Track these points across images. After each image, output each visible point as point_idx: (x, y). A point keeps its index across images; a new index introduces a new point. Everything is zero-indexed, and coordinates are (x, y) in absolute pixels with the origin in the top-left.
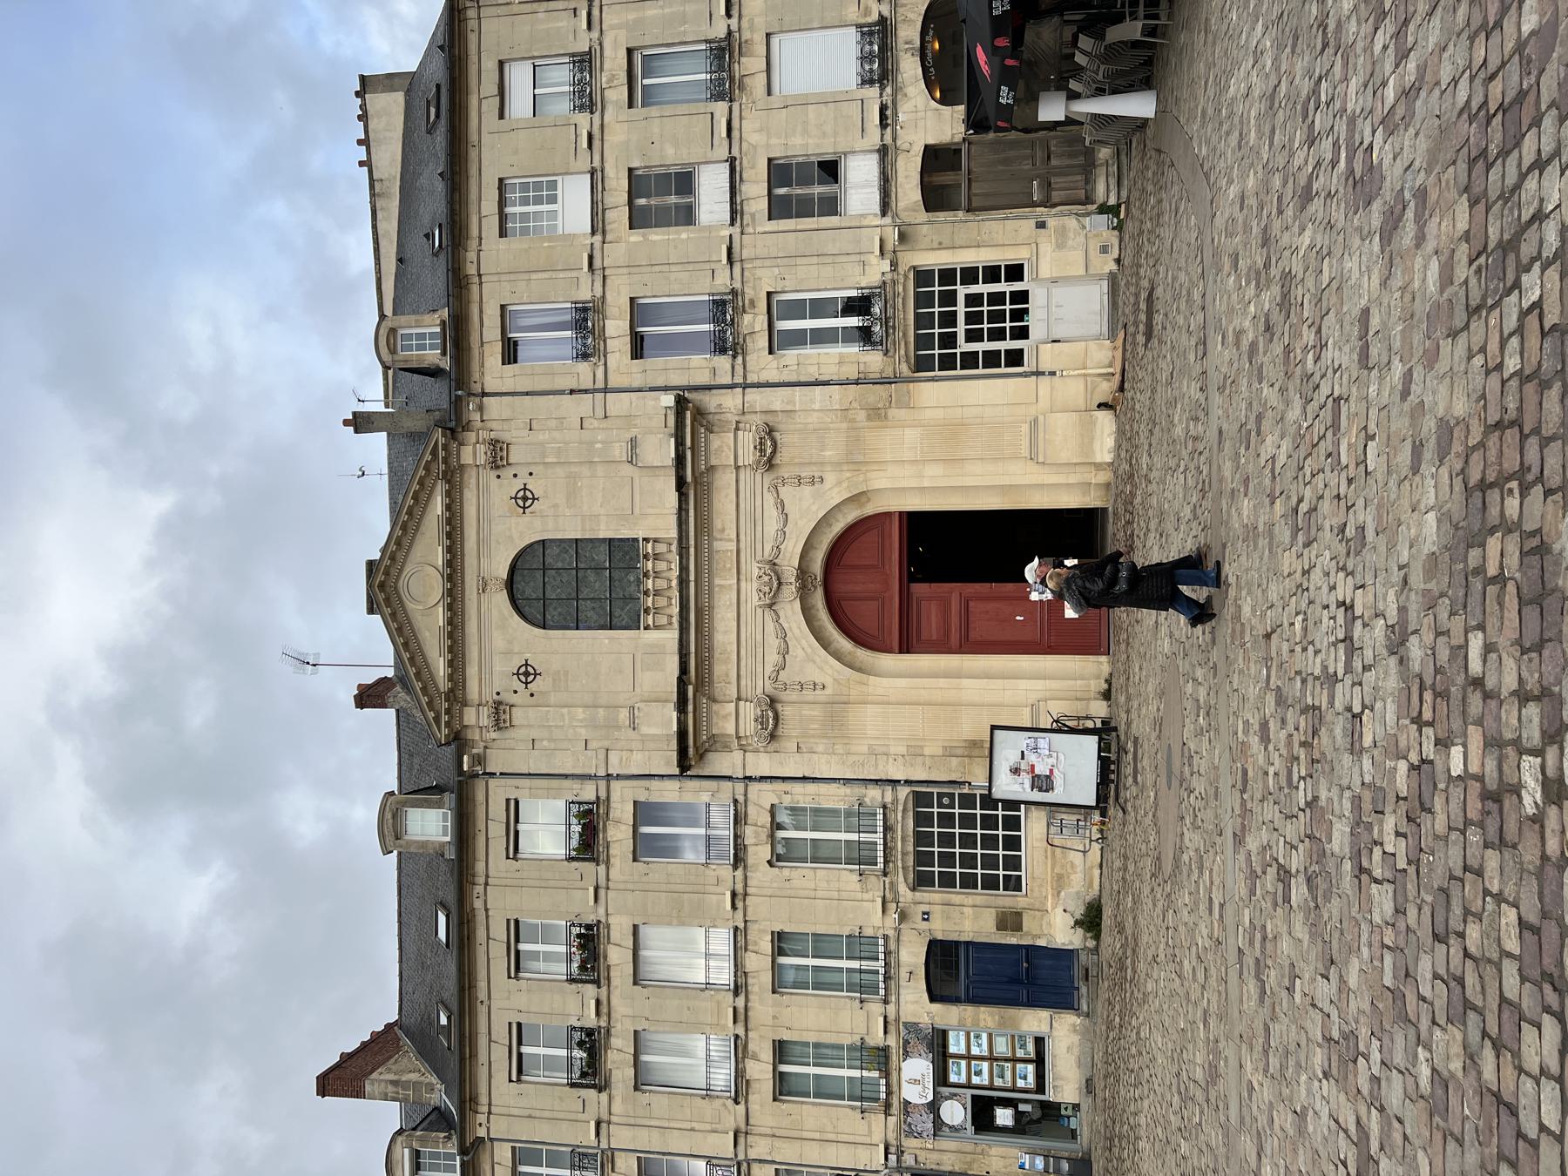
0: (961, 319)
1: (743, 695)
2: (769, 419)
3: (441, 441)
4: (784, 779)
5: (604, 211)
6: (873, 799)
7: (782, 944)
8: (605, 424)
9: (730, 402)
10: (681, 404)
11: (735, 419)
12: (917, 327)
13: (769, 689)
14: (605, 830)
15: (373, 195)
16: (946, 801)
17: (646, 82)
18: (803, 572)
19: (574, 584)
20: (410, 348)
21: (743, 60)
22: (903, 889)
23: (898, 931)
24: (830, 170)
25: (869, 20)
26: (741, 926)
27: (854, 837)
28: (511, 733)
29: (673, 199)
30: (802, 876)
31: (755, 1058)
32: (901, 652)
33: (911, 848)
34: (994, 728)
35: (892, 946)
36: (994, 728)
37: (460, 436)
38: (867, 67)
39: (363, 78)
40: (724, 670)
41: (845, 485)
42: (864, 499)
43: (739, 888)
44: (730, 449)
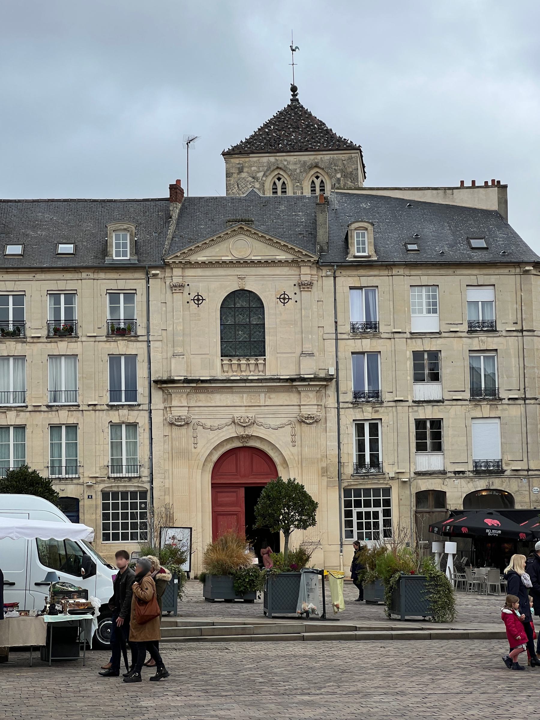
0: (368, 509)
1: (190, 409)
2: (323, 420)
3: (312, 260)
4: (151, 429)
5: (421, 338)
6: (143, 471)
7: (72, 428)
8: (321, 339)
9: (331, 402)
10: (329, 379)
11: (323, 404)
12: (364, 489)
13: (194, 421)
14: (122, 340)
15: (445, 189)
16: (143, 506)
17: (482, 358)
18: (249, 437)
19: (243, 325)
20: (358, 237)
21: (489, 406)
22: (102, 486)
23: (82, 484)
24: (438, 447)
25: (504, 465)
26: (80, 408)
27: (124, 463)
28: (169, 291)
29: (427, 372)
30: (107, 437)
31: (17, 415)
32: (212, 484)
33: (120, 489)
34: (191, 528)
35: (75, 481)
36: (191, 528)
37: (314, 266)
38: (483, 464)
39: (505, 187)
40: (202, 399)
41: (292, 457)
42: (285, 466)
43: (98, 407)
44: (308, 402)
